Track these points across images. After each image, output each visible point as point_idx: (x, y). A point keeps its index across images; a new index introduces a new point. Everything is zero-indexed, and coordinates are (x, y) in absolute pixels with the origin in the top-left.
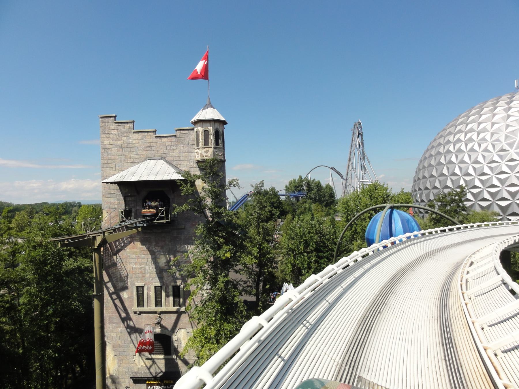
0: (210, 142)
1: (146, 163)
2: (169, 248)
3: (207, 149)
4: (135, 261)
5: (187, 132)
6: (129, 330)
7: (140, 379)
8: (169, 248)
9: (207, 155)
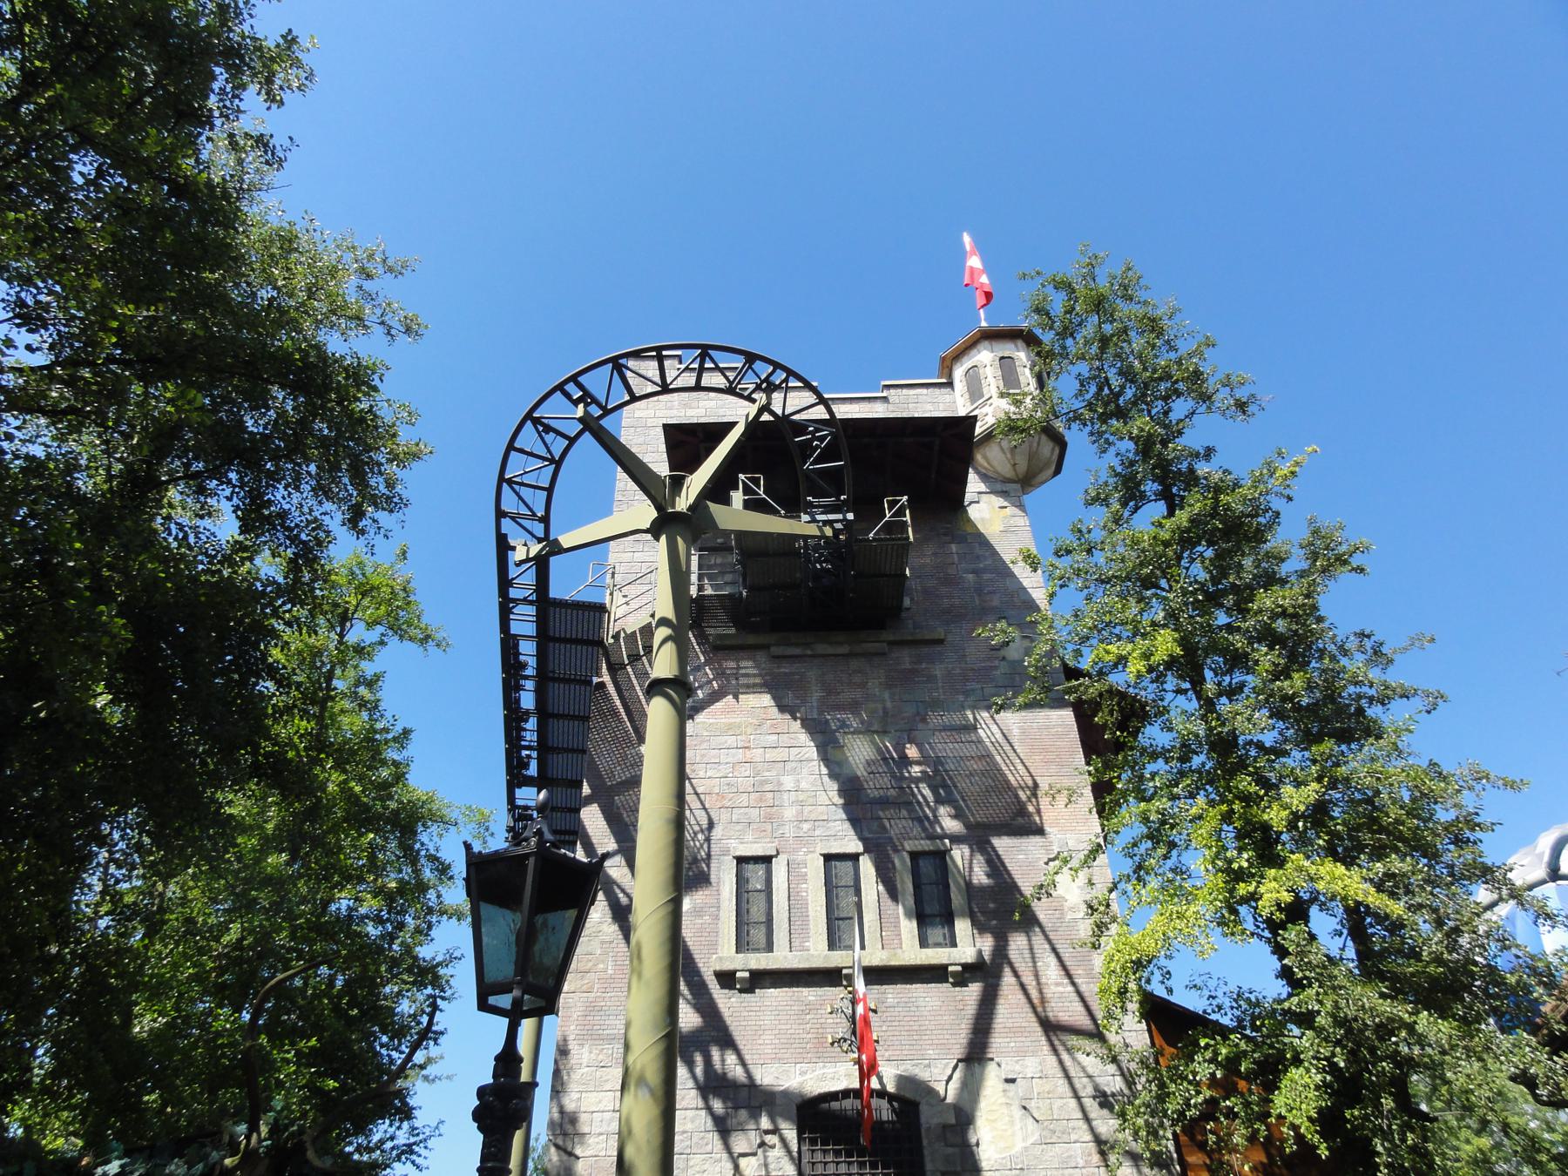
2: (884, 709)
4: (735, 760)
5: (924, 391)
6: (718, 1105)
8: (884, 709)
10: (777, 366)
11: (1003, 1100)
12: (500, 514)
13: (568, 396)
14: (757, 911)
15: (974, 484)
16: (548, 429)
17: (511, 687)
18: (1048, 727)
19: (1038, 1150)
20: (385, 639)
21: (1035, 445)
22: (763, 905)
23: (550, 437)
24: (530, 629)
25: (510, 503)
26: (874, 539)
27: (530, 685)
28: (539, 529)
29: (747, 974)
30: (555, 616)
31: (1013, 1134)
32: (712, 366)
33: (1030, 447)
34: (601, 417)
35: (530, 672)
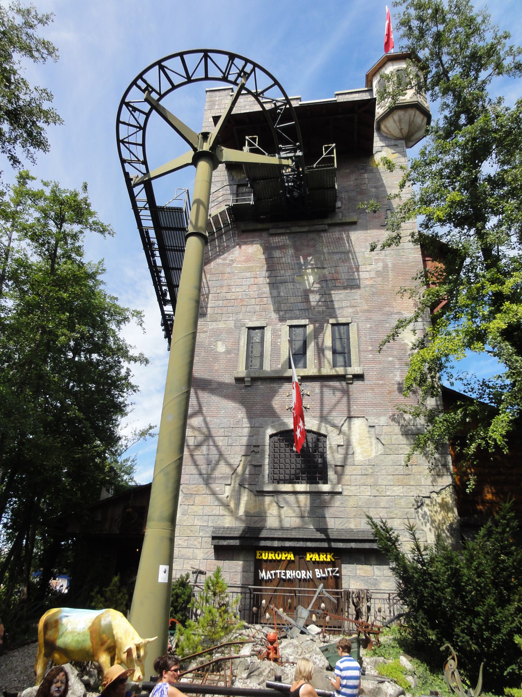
4: (248, 283)
10: (247, 61)
11: (367, 435)
12: (123, 161)
13: (139, 87)
14: (256, 352)
15: (377, 143)
16: (135, 109)
17: (150, 256)
18: (407, 263)
19: (382, 457)
20: (83, 230)
21: (412, 117)
22: (259, 349)
23: (137, 114)
24: (150, 224)
25: (126, 155)
26: (316, 167)
27: (157, 253)
28: (143, 168)
29: (249, 379)
30: (161, 215)
31: (371, 450)
32: (246, 92)
33: (410, 118)
34: (159, 100)
35: (156, 246)
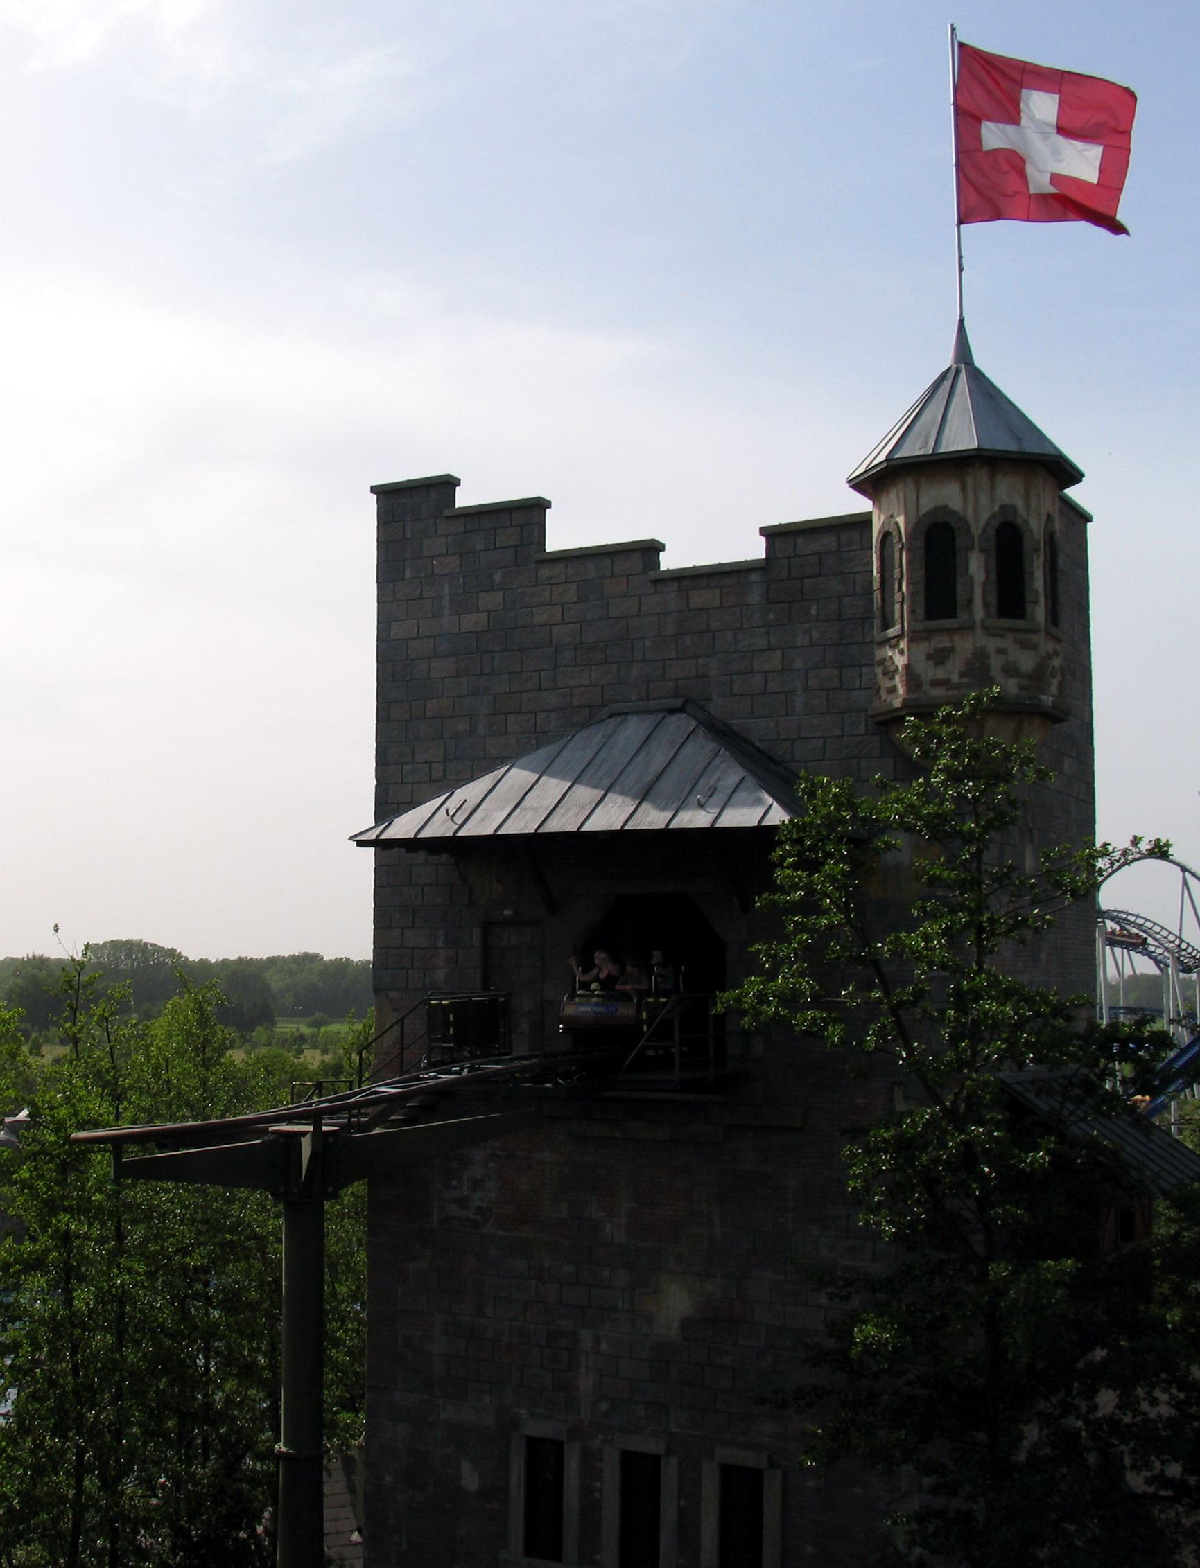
0: (961, 595)
1: (598, 738)
3: (943, 642)
7: (924, 459)
9: (940, 674)
